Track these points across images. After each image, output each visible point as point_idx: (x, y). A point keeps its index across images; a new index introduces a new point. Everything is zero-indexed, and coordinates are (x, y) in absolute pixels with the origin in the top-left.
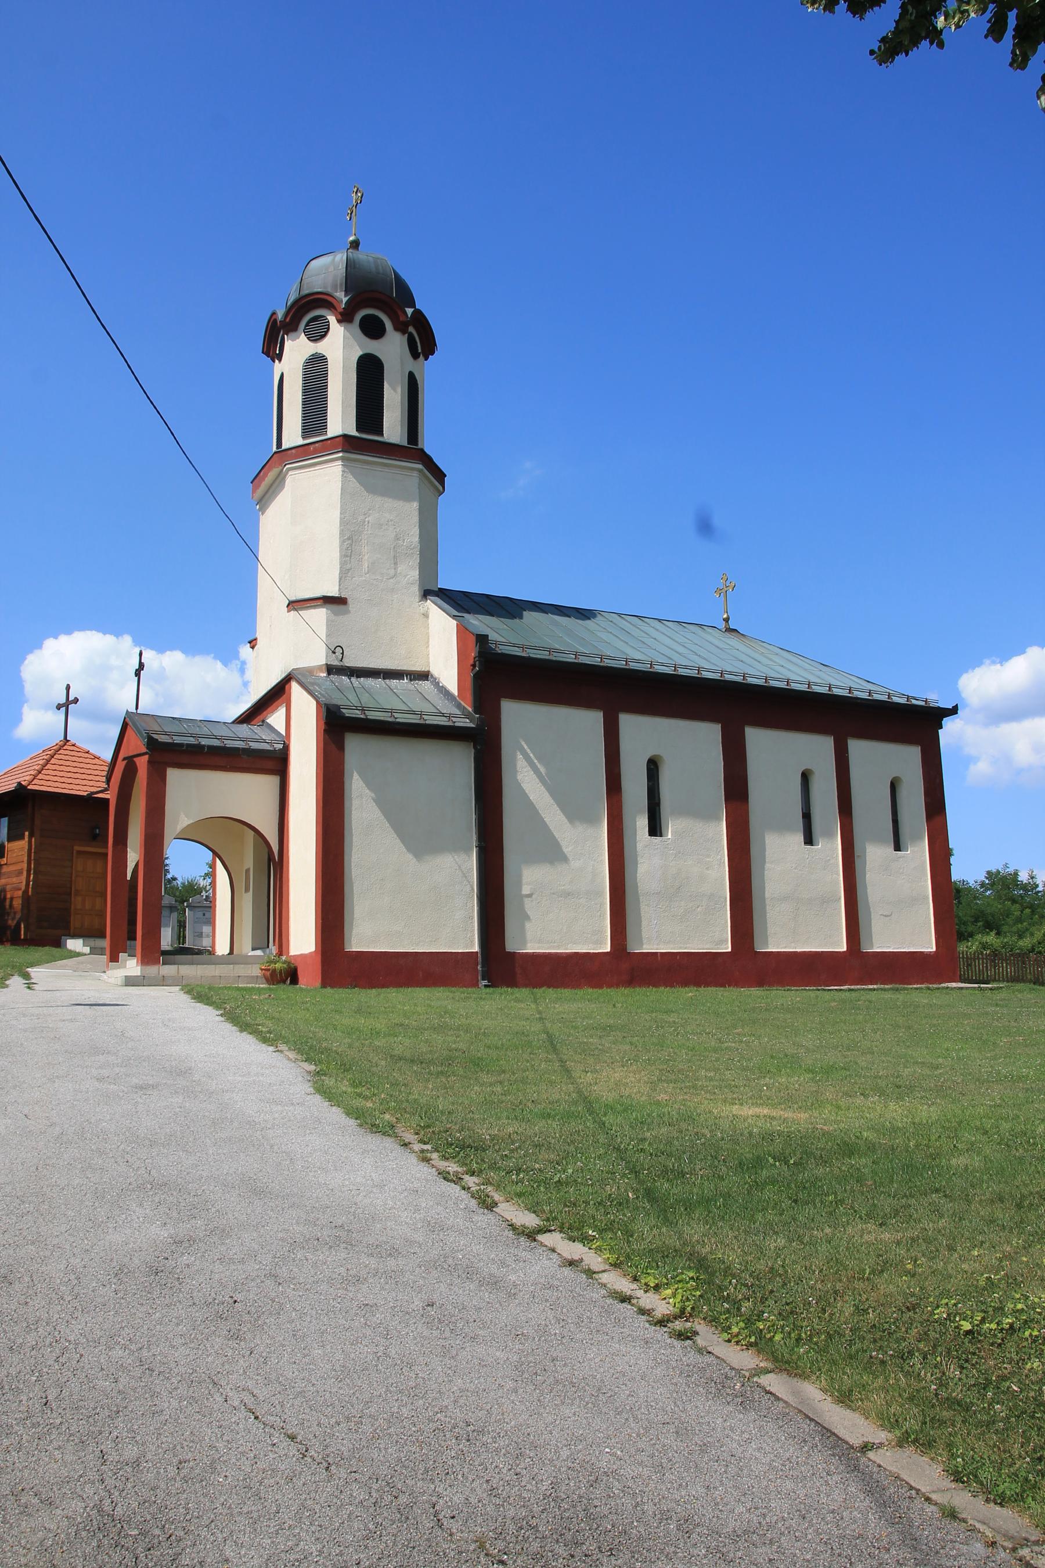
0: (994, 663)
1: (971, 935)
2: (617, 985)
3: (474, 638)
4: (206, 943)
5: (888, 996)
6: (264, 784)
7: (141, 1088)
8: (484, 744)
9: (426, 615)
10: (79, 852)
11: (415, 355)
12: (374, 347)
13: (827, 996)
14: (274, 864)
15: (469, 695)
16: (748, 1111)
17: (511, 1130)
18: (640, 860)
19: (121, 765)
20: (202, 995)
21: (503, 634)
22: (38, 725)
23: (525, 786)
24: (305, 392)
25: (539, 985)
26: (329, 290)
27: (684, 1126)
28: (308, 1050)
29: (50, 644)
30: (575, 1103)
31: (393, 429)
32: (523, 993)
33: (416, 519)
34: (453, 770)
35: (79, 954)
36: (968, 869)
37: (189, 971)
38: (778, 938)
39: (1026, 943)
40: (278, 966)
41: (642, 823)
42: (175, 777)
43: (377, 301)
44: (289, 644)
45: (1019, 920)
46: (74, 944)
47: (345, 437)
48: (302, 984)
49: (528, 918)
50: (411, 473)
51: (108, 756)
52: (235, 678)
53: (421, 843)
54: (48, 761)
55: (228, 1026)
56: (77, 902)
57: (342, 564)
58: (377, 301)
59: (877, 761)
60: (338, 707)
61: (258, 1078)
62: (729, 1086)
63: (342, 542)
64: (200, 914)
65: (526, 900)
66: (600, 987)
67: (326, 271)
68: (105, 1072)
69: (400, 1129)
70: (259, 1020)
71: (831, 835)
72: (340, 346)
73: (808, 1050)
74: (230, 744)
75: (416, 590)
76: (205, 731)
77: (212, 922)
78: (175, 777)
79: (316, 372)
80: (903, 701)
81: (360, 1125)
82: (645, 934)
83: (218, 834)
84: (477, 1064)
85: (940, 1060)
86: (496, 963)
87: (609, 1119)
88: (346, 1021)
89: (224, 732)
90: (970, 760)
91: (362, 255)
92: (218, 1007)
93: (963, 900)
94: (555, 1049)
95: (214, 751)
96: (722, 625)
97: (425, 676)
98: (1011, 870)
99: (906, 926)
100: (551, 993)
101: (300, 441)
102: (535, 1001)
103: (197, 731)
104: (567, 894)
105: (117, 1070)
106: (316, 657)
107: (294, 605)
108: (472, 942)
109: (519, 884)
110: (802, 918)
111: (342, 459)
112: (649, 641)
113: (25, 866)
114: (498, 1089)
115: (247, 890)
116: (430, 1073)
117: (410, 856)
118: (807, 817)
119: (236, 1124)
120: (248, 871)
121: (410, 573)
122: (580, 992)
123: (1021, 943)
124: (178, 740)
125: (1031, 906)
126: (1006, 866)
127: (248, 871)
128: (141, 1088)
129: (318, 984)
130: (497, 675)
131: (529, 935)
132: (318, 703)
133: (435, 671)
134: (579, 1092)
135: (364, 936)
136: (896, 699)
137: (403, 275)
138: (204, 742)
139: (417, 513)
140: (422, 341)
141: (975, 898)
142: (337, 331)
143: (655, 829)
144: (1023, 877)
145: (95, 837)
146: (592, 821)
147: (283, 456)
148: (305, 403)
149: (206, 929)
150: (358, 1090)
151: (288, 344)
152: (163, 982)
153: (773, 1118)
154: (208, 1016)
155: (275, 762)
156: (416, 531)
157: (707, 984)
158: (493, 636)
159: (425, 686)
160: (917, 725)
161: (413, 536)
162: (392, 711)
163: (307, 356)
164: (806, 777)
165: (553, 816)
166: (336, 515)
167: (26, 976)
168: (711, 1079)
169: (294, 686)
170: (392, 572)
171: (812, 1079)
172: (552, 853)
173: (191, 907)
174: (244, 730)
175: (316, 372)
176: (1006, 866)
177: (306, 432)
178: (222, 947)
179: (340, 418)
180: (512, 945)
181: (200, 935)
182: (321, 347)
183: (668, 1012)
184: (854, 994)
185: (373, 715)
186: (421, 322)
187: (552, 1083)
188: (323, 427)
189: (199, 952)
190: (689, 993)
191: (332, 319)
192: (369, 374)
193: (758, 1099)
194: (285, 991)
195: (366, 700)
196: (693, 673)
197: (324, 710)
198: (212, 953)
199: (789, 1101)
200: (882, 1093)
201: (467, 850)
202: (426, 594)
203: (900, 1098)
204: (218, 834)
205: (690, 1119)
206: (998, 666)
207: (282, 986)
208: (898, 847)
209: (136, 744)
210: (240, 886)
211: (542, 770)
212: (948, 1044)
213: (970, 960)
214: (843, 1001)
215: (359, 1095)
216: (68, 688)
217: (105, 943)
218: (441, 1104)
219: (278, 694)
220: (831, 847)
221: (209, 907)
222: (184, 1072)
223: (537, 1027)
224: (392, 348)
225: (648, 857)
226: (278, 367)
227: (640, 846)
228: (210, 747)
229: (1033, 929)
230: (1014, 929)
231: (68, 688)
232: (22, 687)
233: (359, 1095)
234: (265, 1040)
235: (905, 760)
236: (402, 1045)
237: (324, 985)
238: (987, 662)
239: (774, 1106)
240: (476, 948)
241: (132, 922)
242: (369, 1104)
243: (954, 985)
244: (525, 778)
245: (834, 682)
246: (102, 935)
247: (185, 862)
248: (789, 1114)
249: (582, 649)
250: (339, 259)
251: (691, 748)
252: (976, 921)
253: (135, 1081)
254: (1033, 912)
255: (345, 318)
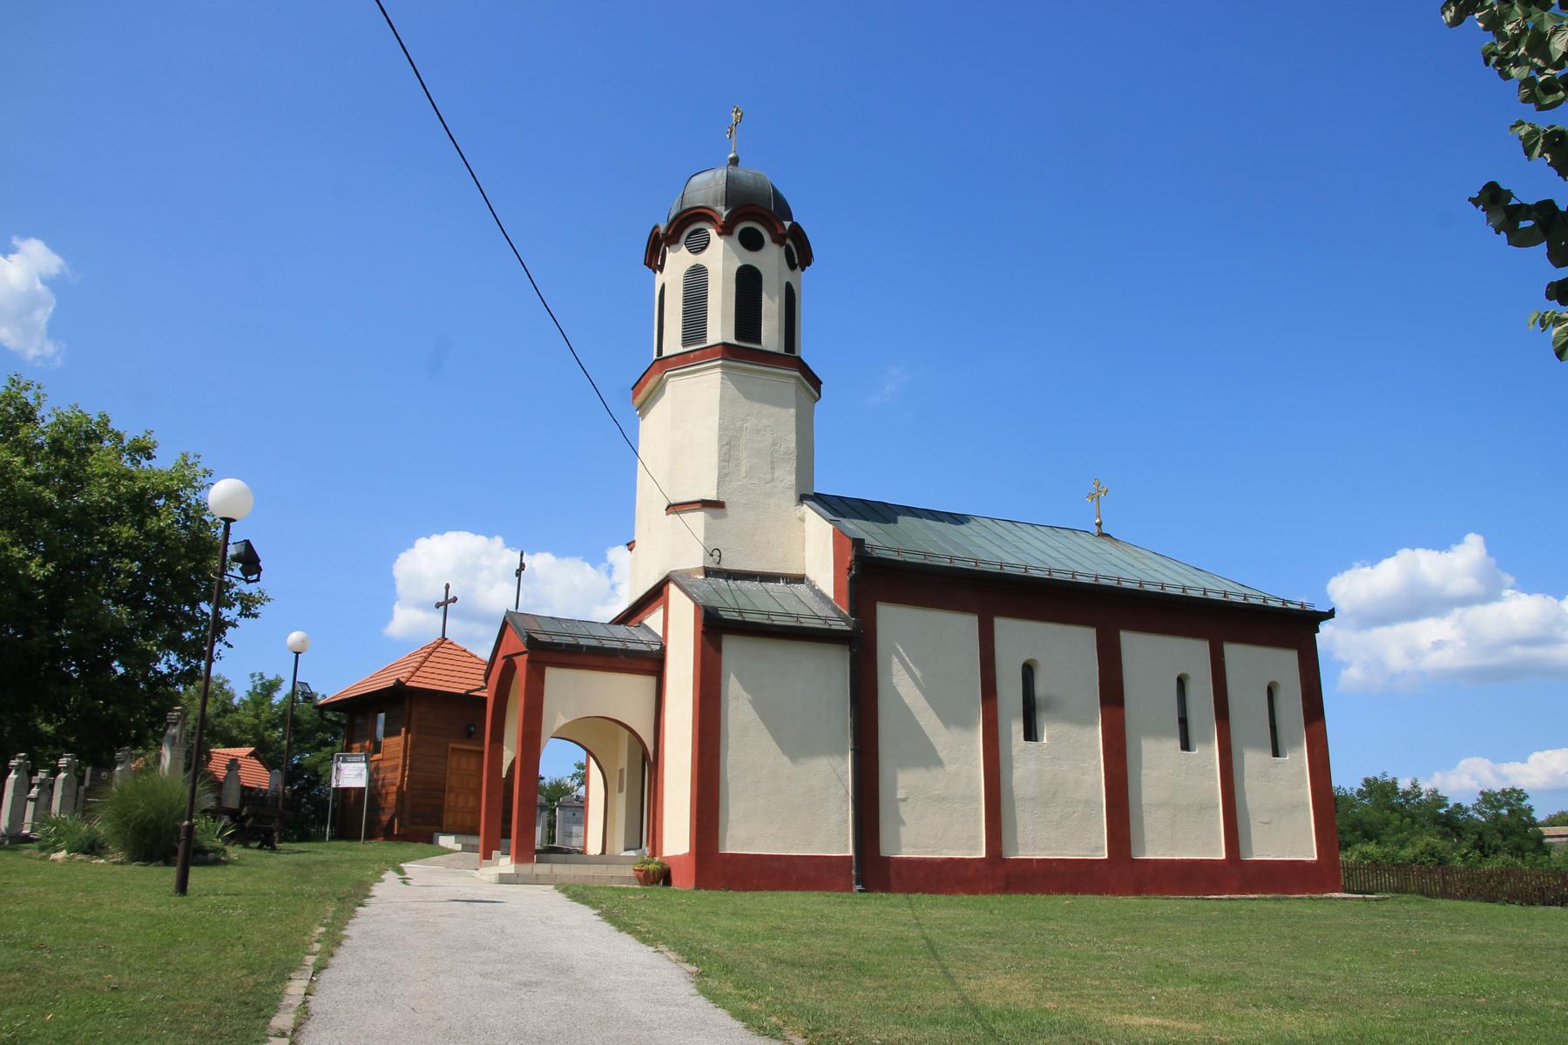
0: (1364, 566)
1: (1349, 845)
2: (992, 892)
3: (850, 543)
4: (575, 843)
5: (1270, 905)
6: (645, 683)
7: (525, 985)
8: (859, 647)
9: (802, 520)
10: (454, 750)
11: (792, 266)
12: (753, 259)
13: (1207, 905)
14: (648, 763)
15: (845, 599)
16: (1140, 1020)
17: (900, 1035)
18: (1015, 765)
19: (499, 663)
20: (578, 894)
21: (878, 538)
22: (411, 623)
23: (900, 690)
24: (685, 301)
25: (916, 891)
26: (710, 204)
27: (1075, 1034)
28: (688, 951)
29: (422, 544)
30: (962, 1010)
31: (771, 336)
32: (899, 898)
33: (792, 425)
34: (828, 672)
35: (450, 851)
36: (1347, 778)
37: (561, 869)
38: (1158, 843)
39: (1408, 853)
40: (651, 867)
41: (1017, 728)
42: (553, 676)
43: (756, 215)
44: (668, 546)
45: (1399, 830)
46: (446, 841)
47: (725, 345)
48: (675, 885)
49: (902, 822)
50: (788, 381)
51: (485, 654)
52: (604, 582)
53: (796, 746)
54: (426, 659)
55: (607, 925)
56: (450, 799)
57: (721, 468)
58: (756, 215)
59: (1253, 666)
60: (716, 609)
61: (640, 976)
62: (1116, 995)
63: (721, 447)
64: (569, 814)
65: (901, 805)
66: (975, 893)
67: (707, 187)
68: (488, 968)
69: (787, 1032)
70: (638, 920)
71: (1295, 744)
72: (720, 258)
73: (1193, 960)
74: (608, 644)
75: (792, 494)
76: (584, 631)
77: (583, 822)
78: (553, 676)
79: (696, 280)
80: (1278, 605)
81: (747, 1028)
82: (1020, 840)
83: (594, 734)
84: (859, 969)
85: (1332, 972)
86: (871, 868)
87: (999, 1026)
88: (724, 923)
89: (602, 632)
90: (1341, 665)
91: (741, 171)
92: (594, 907)
93: (1340, 808)
94: (936, 956)
95: (592, 651)
96: (1095, 530)
97: (800, 579)
98: (1389, 779)
99: (1285, 834)
100: (926, 899)
101: (681, 350)
102: (911, 907)
103: (575, 630)
104: (942, 799)
105: (499, 966)
106: (693, 559)
107: (674, 508)
108: (847, 846)
109: (894, 789)
110: (1179, 828)
111: (722, 366)
112: (1023, 546)
113: (401, 761)
114: (883, 994)
115: (621, 790)
116: (812, 977)
117: (785, 759)
118: (1183, 722)
119: (622, 1023)
120: (621, 771)
121: (787, 477)
122: (956, 898)
123: (1402, 853)
124: (557, 639)
125: (1412, 816)
126: (1384, 774)
127: (621, 771)
128: (525, 985)
129: (692, 884)
130: (874, 579)
131: (904, 840)
132: (696, 605)
133: (811, 574)
134: (964, 999)
135: (738, 839)
136: (1271, 603)
137: (782, 191)
138: (582, 642)
139: (793, 419)
140: (799, 253)
141: (1353, 806)
142: (717, 243)
143: (1030, 734)
144: (1404, 784)
145: (470, 735)
146: (967, 725)
147: (664, 363)
148: (685, 312)
149: (575, 829)
150: (743, 992)
151: (670, 256)
152: (536, 880)
153: (1166, 1028)
154: (583, 916)
155: (652, 663)
156: (793, 437)
157: (1084, 892)
158: (869, 540)
159: (801, 589)
160: (1295, 628)
161: (790, 442)
162: (769, 614)
163: (688, 267)
164: (1181, 682)
165: (927, 719)
166: (714, 420)
167: (400, 871)
168: (1097, 988)
169: (672, 588)
170: (769, 477)
171: (1201, 990)
172: (928, 757)
173: (561, 806)
174: (621, 631)
175: (696, 280)
176: (1384, 774)
177: (687, 340)
178: (594, 848)
179: (720, 328)
180: (886, 850)
181: (570, 835)
182: (702, 259)
183: (1045, 919)
184: (1235, 904)
185: (750, 618)
186: (798, 234)
187: (936, 989)
188: (702, 336)
189: (569, 852)
190: (1066, 900)
191: (712, 232)
192: (748, 285)
193: (1148, 1008)
194: (659, 891)
195: (743, 603)
196: (1068, 577)
197: (702, 612)
198: (583, 852)
199: (1179, 1011)
200: (1276, 1005)
201: (843, 754)
202: (802, 498)
203: (1295, 1009)
204: (594, 734)
205: (1081, 1026)
206: (1368, 569)
207: (656, 887)
208: (1276, 753)
209: (515, 643)
210: (614, 785)
211: (918, 673)
212: (1337, 956)
213: (1351, 870)
214: (1224, 910)
215: (744, 997)
216: (447, 587)
217: (479, 841)
218: (827, 1008)
219: (655, 596)
220: (1209, 753)
221: (582, 805)
222: (563, 969)
223: (915, 933)
224: (770, 260)
225: (1026, 763)
226: (659, 278)
227: (1015, 751)
228: (589, 648)
229: (1413, 839)
230: (1394, 838)
231: (447, 587)
232: (394, 586)
233: (744, 997)
234: (644, 940)
235: (1282, 664)
236: (782, 948)
237: (698, 886)
238: (1357, 564)
239: (1164, 1016)
240: (850, 853)
241: (507, 820)
242: (755, 1007)
243: (1337, 895)
244: (901, 682)
245: (1208, 586)
246: (475, 833)
247: (558, 762)
248: (1180, 1024)
249: (956, 554)
250: (720, 175)
251: (1065, 652)
252: (1355, 830)
253: (518, 977)
254: (1413, 822)
255: (725, 231)
